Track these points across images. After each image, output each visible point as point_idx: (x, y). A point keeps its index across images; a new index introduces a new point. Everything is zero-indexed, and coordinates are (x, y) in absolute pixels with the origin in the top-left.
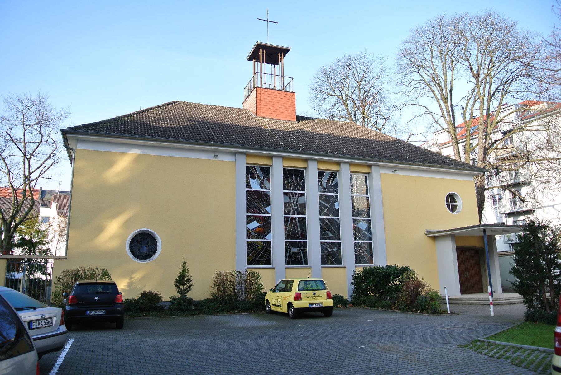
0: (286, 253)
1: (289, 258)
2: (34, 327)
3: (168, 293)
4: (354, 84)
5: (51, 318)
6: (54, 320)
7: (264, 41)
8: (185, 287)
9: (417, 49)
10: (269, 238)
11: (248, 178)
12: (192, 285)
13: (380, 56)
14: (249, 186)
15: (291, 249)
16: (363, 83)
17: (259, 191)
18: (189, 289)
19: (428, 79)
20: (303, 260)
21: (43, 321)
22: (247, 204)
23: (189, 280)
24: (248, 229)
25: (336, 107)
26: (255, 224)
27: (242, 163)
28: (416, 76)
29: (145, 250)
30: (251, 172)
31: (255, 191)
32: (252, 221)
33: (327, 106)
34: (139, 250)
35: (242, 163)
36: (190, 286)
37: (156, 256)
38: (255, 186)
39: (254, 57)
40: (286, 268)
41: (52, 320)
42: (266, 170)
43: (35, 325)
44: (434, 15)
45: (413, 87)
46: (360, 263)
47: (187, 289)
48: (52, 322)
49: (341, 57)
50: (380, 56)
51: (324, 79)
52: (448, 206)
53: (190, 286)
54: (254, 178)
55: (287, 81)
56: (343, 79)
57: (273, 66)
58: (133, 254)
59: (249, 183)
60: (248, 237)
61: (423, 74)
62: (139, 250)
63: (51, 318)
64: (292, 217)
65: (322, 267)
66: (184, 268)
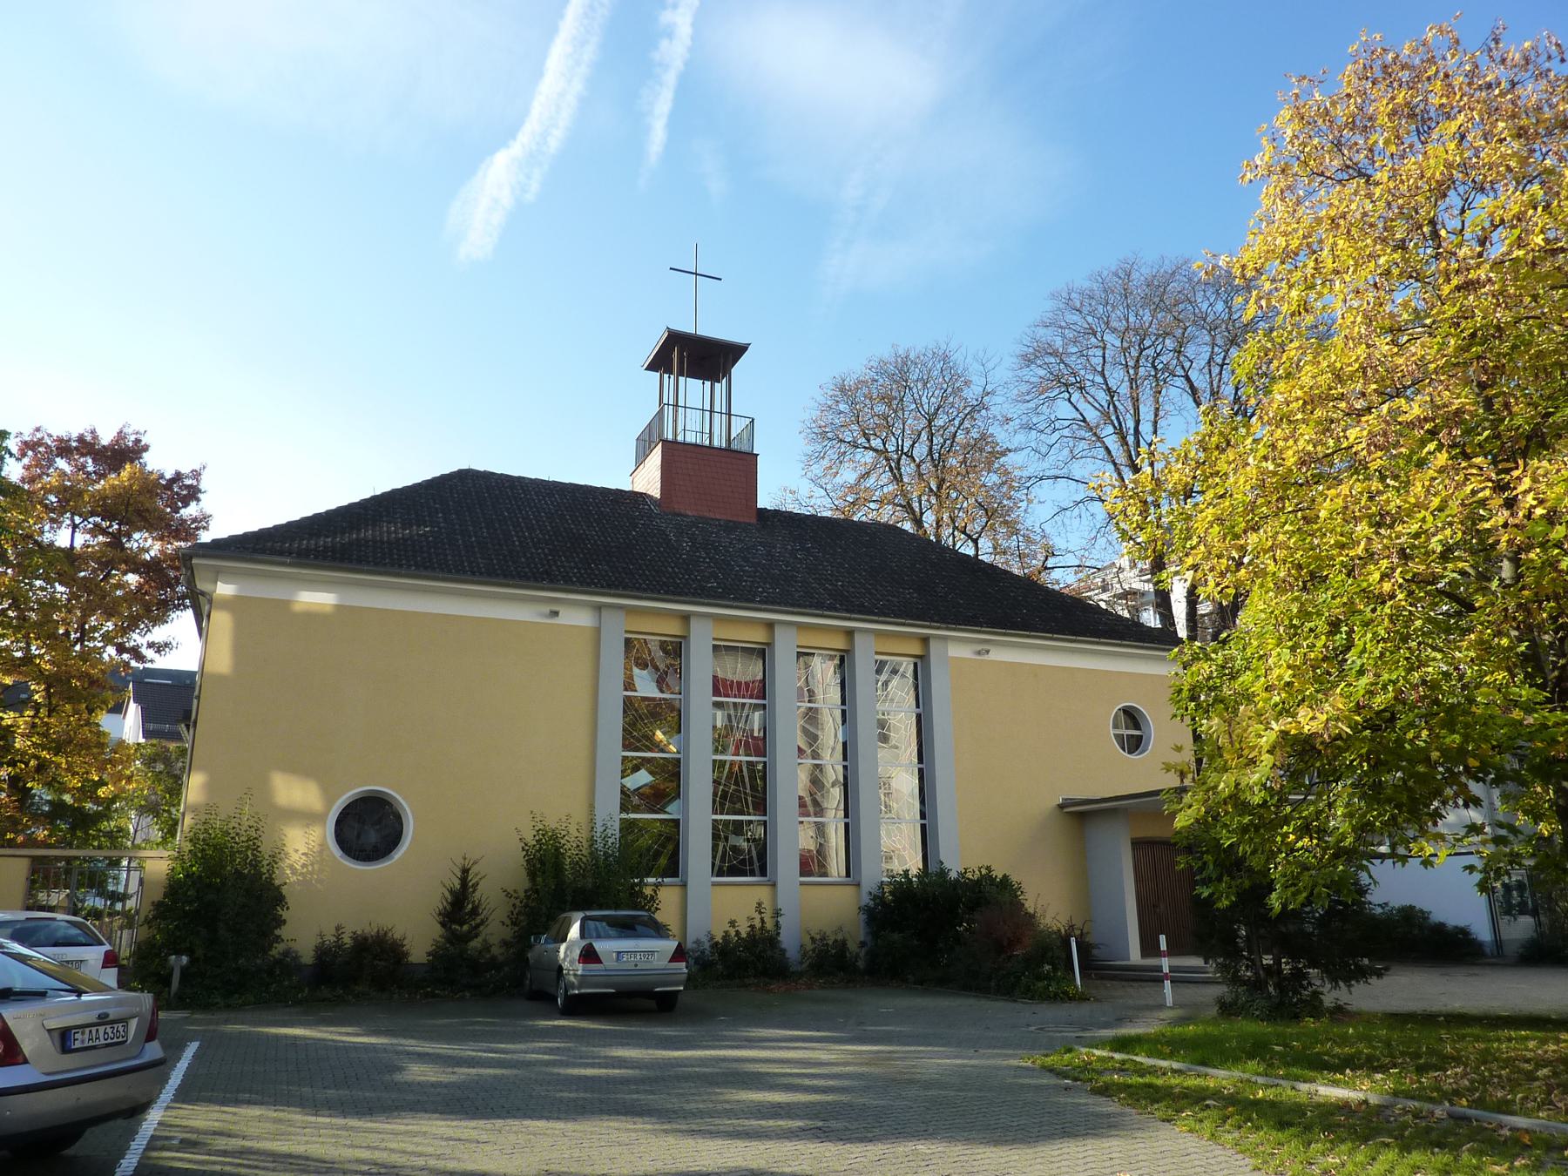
0: (715, 848)
1: (723, 859)
2: (78, 1045)
3: (419, 935)
4: (915, 423)
5: (124, 1020)
6: (133, 1024)
7: (687, 327)
8: (466, 927)
9: (1065, 346)
10: (673, 811)
11: (628, 669)
12: (482, 922)
13: (981, 354)
14: (629, 685)
15: (726, 839)
16: (939, 422)
17: (653, 699)
18: (474, 933)
19: (1092, 415)
20: (756, 865)
21: (102, 1029)
22: (624, 730)
23: (475, 912)
24: (624, 792)
25: (870, 482)
26: (643, 778)
27: (616, 629)
28: (1063, 410)
29: (372, 837)
30: (634, 651)
31: (644, 699)
32: (636, 769)
33: (848, 476)
34: (359, 836)
35: (616, 629)
36: (478, 926)
37: (398, 854)
38: (646, 686)
39: (660, 363)
40: (714, 884)
41: (126, 1027)
42: (676, 650)
43: (80, 1040)
44: (1108, 261)
45: (1057, 435)
46: (810, 874)
47: (469, 932)
48: (126, 1032)
49: (886, 353)
50: (981, 354)
51: (842, 407)
52: (1119, 738)
53: (478, 926)
54: (644, 666)
55: (738, 426)
56: (885, 406)
57: (708, 384)
58: (342, 848)
59: (631, 677)
60: (624, 809)
61: (1082, 406)
62: (359, 836)
63: (124, 1020)
64: (732, 763)
65: (802, 884)
66: (464, 881)
